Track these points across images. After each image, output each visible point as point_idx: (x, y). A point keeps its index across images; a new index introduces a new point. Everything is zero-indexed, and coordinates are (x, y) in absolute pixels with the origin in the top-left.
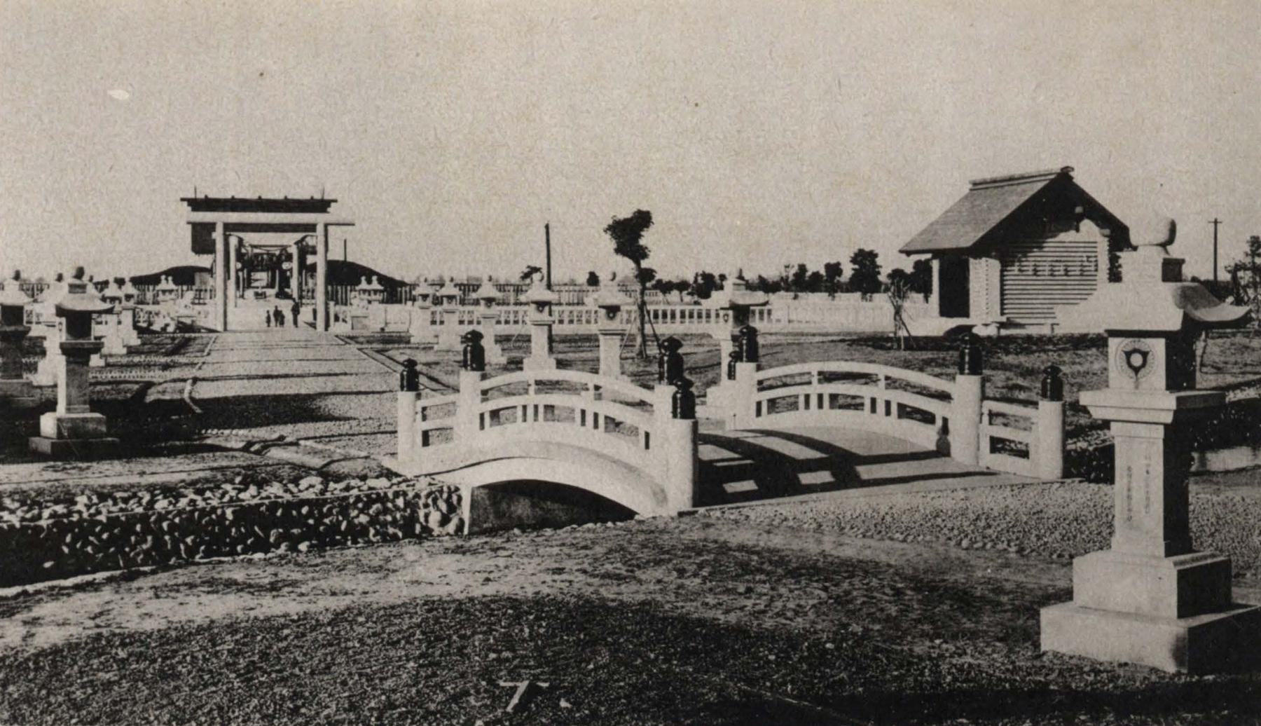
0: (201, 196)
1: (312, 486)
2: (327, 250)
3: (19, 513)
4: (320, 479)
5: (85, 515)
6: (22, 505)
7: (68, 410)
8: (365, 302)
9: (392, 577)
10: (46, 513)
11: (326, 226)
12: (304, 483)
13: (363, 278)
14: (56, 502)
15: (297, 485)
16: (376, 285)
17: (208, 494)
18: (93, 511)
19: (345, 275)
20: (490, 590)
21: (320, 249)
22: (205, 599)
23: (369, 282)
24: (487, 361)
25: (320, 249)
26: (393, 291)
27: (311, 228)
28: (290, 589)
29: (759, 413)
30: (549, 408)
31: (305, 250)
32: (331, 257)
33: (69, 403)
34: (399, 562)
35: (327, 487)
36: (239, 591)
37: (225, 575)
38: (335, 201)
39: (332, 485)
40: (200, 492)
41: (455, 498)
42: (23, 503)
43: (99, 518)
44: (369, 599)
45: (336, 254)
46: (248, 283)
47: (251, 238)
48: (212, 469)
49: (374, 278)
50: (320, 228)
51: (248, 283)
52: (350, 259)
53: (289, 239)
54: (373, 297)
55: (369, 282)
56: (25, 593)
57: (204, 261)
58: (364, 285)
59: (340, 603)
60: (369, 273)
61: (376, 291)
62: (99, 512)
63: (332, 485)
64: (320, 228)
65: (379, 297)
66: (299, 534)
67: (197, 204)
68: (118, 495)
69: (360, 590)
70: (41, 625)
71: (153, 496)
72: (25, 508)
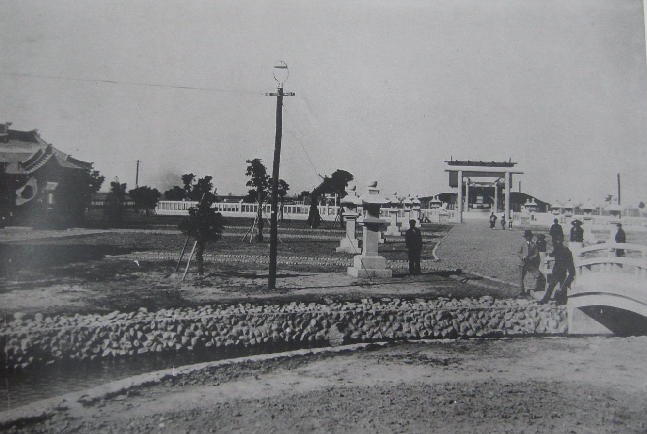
0: (454, 160)
1: (486, 301)
2: (511, 187)
3: (332, 306)
4: (491, 297)
5: (364, 309)
6: (334, 302)
7: (367, 254)
8: (528, 212)
9: (520, 362)
10: (345, 307)
11: (511, 174)
12: (482, 300)
13: (528, 200)
14: (351, 302)
15: (478, 300)
16: (533, 203)
17: (430, 302)
18: (368, 307)
19: (518, 199)
20: (578, 377)
21: (507, 186)
22: (406, 367)
23: (530, 201)
24: (564, 234)
25: (507, 186)
26: (542, 207)
27: (502, 175)
28: (455, 365)
29: (453, 214)
30: (620, 265)
31: (501, 187)
32: (512, 190)
33: (368, 250)
34: (525, 352)
35: (494, 301)
36: (426, 363)
37: (422, 353)
38: (515, 164)
39: (497, 301)
40: (427, 301)
41: (564, 313)
42: (335, 301)
43: (370, 311)
44: (501, 376)
45: (515, 189)
46: (475, 201)
47: (474, 179)
48: (435, 288)
49: (533, 199)
50: (507, 175)
51: (475, 201)
52: (521, 192)
53: (492, 180)
54: (532, 209)
55: (530, 201)
56: (311, 353)
57: (452, 191)
58: (528, 203)
59: (484, 377)
60: (530, 198)
61: (533, 206)
62: (371, 308)
63: (497, 301)
64: (507, 175)
65: (534, 209)
66: (570, 272)
67: (451, 163)
68: (384, 299)
69: (498, 369)
70: (307, 376)
71: (401, 301)
72: (335, 304)
